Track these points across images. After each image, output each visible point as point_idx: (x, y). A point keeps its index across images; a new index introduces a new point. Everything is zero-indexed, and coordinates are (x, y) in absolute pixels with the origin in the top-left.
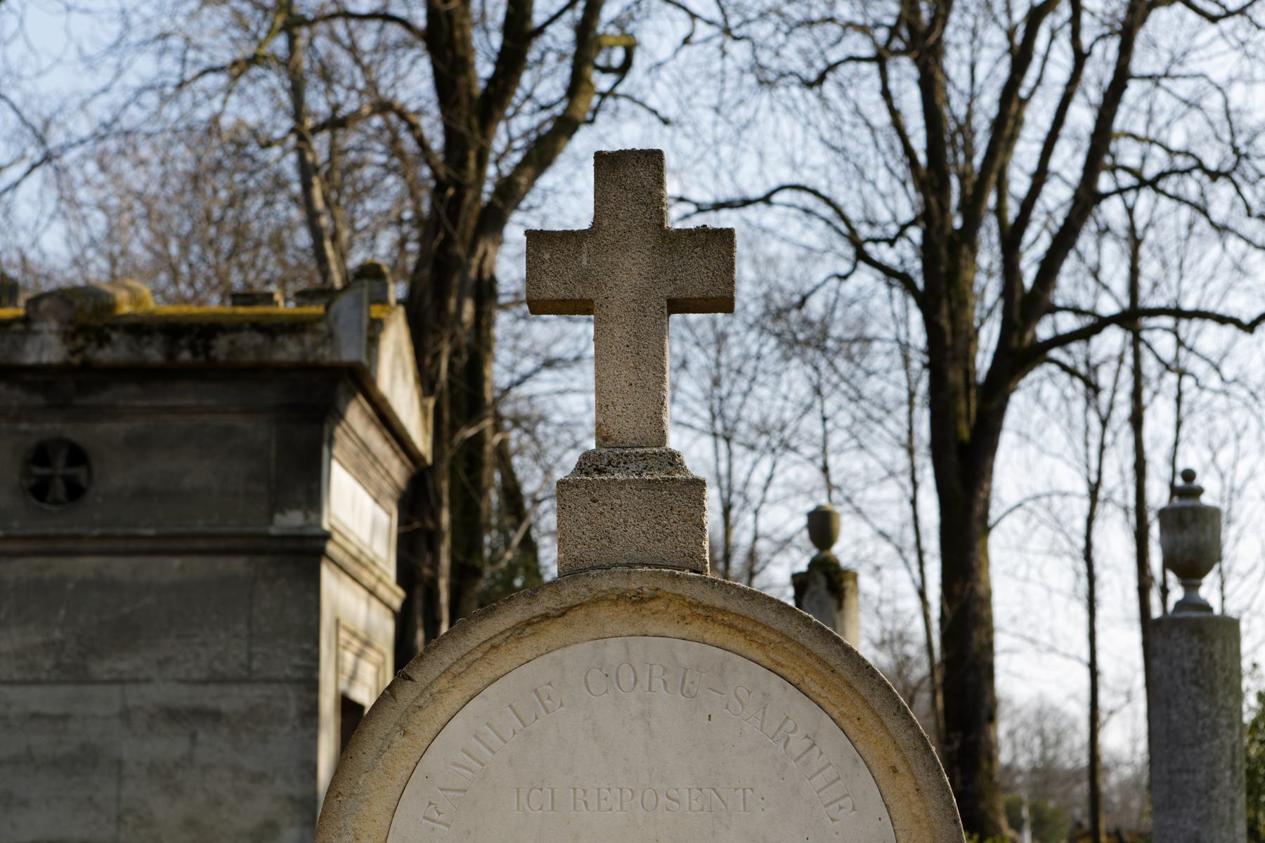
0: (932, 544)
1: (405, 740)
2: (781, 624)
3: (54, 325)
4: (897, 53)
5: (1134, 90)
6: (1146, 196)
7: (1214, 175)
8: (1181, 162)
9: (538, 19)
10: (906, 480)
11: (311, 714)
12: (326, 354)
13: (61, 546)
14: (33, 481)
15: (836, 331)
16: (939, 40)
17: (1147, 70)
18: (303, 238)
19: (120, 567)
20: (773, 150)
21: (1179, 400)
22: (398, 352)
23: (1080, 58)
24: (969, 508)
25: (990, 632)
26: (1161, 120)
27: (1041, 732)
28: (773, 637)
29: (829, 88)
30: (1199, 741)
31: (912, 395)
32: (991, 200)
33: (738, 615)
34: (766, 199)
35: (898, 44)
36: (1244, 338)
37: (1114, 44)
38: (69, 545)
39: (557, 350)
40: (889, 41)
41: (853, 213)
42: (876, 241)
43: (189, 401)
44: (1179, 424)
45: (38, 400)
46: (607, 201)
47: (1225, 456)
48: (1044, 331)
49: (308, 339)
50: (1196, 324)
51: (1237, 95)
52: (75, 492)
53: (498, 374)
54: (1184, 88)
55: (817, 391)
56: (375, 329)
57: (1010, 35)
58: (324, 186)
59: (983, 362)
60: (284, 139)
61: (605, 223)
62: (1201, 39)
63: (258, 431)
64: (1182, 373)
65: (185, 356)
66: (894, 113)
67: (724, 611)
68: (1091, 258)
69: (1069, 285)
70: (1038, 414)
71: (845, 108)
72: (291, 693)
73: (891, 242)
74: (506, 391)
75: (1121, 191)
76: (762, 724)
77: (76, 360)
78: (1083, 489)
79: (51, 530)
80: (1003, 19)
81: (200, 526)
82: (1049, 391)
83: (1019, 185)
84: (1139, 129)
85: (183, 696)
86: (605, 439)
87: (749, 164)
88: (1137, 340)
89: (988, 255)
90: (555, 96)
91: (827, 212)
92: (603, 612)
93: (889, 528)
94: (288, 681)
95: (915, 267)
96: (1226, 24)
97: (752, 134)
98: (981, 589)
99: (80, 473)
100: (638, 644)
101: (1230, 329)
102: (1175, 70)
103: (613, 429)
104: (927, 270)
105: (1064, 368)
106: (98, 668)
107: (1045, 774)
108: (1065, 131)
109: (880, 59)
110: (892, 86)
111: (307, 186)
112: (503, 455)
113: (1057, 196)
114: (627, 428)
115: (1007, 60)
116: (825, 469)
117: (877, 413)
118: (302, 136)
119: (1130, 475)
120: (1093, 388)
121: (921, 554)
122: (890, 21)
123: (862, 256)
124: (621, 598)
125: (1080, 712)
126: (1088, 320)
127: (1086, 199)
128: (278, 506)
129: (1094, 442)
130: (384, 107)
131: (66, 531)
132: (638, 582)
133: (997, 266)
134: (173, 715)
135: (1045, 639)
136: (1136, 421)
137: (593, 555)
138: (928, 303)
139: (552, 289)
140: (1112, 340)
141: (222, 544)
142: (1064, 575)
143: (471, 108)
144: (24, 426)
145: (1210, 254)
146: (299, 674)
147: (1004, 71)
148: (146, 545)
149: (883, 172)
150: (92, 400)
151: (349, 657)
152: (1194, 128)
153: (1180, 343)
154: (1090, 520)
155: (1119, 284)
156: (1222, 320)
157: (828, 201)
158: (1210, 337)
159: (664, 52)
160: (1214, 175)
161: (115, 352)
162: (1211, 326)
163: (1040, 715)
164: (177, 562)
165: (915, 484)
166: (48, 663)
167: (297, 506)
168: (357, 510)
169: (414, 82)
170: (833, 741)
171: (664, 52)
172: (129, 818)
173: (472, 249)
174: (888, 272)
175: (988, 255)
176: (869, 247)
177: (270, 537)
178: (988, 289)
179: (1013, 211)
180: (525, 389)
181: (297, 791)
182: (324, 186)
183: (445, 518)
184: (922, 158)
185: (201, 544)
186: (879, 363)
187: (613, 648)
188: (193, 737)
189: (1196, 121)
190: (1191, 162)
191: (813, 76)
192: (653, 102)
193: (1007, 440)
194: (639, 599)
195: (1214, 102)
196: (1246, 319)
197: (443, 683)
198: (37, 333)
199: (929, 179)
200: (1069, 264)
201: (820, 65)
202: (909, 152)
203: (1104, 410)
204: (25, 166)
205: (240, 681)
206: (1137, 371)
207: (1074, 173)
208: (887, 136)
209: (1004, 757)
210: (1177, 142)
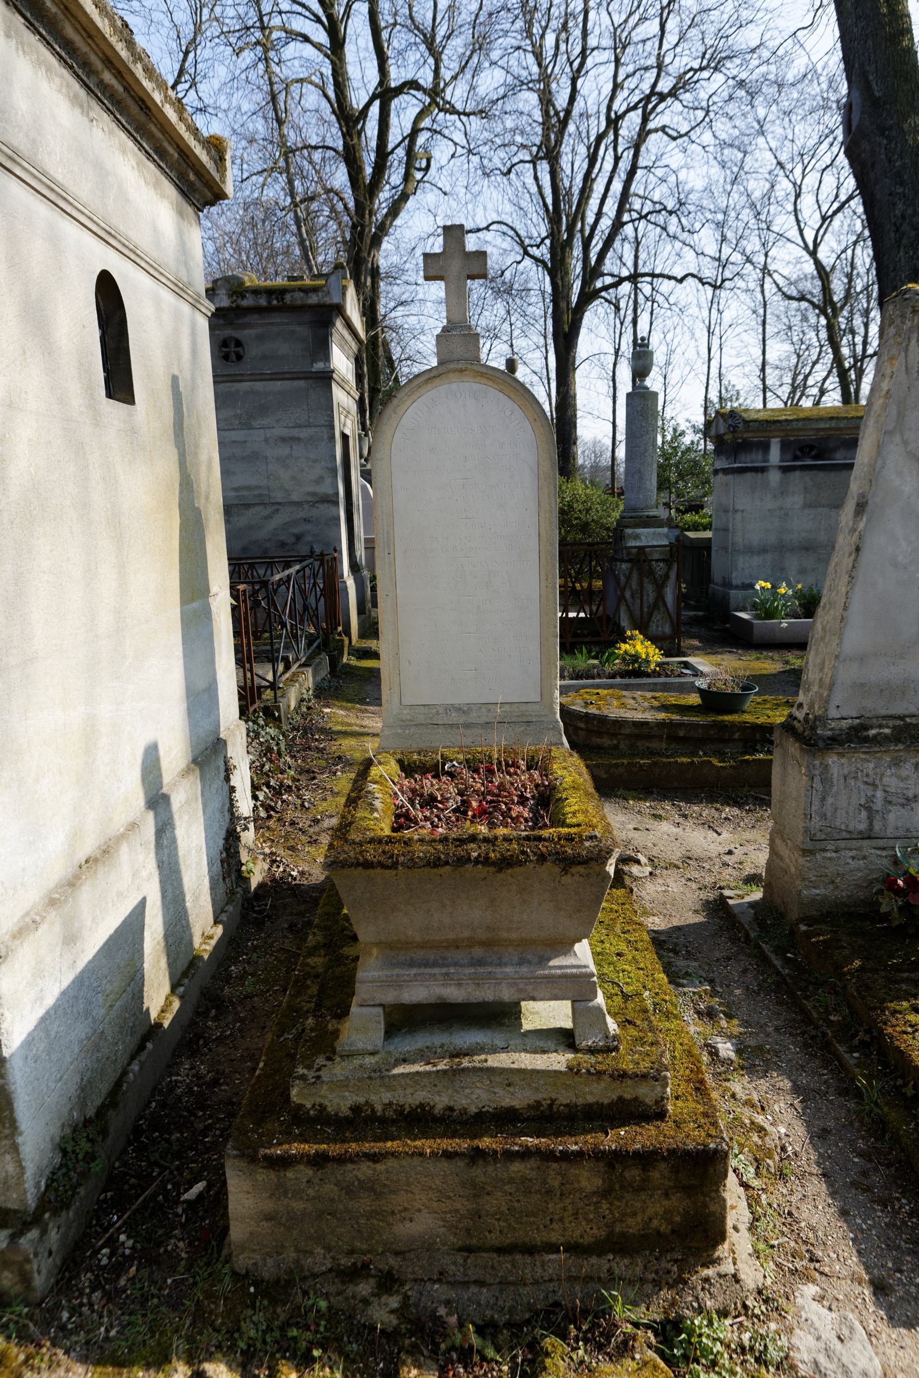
0: (553, 375)
2: (503, 377)
4: (541, 158)
5: (640, 173)
6: (643, 222)
7: (670, 213)
9: (390, 146)
10: (544, 350)
11: (333, 437)
12: (327, 300)
15: (516, 286)
16: (558, 152)
17: (644, 165)
18: (297, 251)
19: (259, 386)
20: (490, 206)
21: (652, 313)
23: (617, 159)
24: (567, 360)
25: (575, 410)
26: (650, 187)
27: (594, 452)
29: (512, 176)
30: (642, 436)
31: (546, 313)
32: (579, 225)
34: (487, 228)
36: (679, 286)
37: (632, 152)
39: (404, 298)
40: (538, 152)
41: (522, 233)
42: (532, 246)
44: (651, 324)
47: (669, 337)
48: (599, 284)
49: (320, 294)
50: (660, 279)
51: (682, 175)
52: (239, 357)
53: (381, 310)
55: (508, 312)
56: (344, 288)
57: (589, 148)
58: (305, 226)
59: (574, 299)
62: (669, 148)
63: (304, 331)
64: (653, 302)
65: (275, 302)
66: (540, 187)
69: (610, 265)
70: (596, 320)
71: (519, 184)
73: (538, 246)
74: (385, 316)
75: (633, 221)
76: (497, 402)
78: (612, 351)
80: (586, 140)
81: (286, 369)
82: (601, 310)
83: (590, 219)
84: (641, 193)
85: (286, 433)
87: (480, 212)
88: (636, 288)
89: (577, 251)
90: (398, 182)
91: (512, 233)
92: (451, 375)
93: (536, 370)
95: (547, 257)
96: (679, 141)
97: (481, 199)
98: (572, 393)
99: (239, 349)
101: (673, 282)
104: (552, 258)
105: (606, 300)
106: (255, 424)
107: (596, 468)
108: (610, 194)
109: (533, 162)
110: (539, 174)
111: (299, 228)
112: (386, 344)
113: (606, 223)
114: (456, 317)
116: (512, 346)
117: (532, 322)
120: (617, 308)
121: (549, 379)
122: (538, 143)
123: (526, 253)
124: (456, 370)
125: (609, 442)
127: (618, 225)
128: (314, 361)
129: (618, 332)
130: (328, 191)
132: (461, 365)
133: (581, 256)
134: (283, 440)
135: (595, 412)
136: (635, 322)
138: (552, 273)
139: (432, 273)
140: (626, 287)
142: (604, 387)
143: (365, 190)
145: (667, 248)
147: (585, 165)
149: (535, 214)
150: (241, 321)
151: (342, 417)
152: (664, 190)
153: (653, 289)
154: (615, 364)
155: (630, 264)
156: (670, 278)
157: (512, 228)
158: (666, 286)
159: (444, 162)
160: (670, 213)
162: (666, 281)
163: (595, 443)
164: (279, 383)
165: (547, 352)
168: (342, 362)
169: (340, 177)
170: (518, 412)
171: (444, 162)
173: (369, 254)
174: (536, 260)
175: (577, 251)
178: (576, 267)
179: (587, 233)
180: (393, 315)
181: (329, 465)
182: (305, 226)
183: (365, 369)
184: (551, 208)
185: (288, 376)
186: (533, 300)
187: (454, 386)
189: (664, 188)
192: (440, 185)
193: (583, 331)
194: (461, 371)
195: (672, 179)
199: (554, 218)
200: (610, 254)
201: (508, 165)
202: (545, 205)
205: (306, 426)
206: (636, 302)
207: (613, 214)
208: (537, 198)
209: (580, 461)
210: (656, 199)
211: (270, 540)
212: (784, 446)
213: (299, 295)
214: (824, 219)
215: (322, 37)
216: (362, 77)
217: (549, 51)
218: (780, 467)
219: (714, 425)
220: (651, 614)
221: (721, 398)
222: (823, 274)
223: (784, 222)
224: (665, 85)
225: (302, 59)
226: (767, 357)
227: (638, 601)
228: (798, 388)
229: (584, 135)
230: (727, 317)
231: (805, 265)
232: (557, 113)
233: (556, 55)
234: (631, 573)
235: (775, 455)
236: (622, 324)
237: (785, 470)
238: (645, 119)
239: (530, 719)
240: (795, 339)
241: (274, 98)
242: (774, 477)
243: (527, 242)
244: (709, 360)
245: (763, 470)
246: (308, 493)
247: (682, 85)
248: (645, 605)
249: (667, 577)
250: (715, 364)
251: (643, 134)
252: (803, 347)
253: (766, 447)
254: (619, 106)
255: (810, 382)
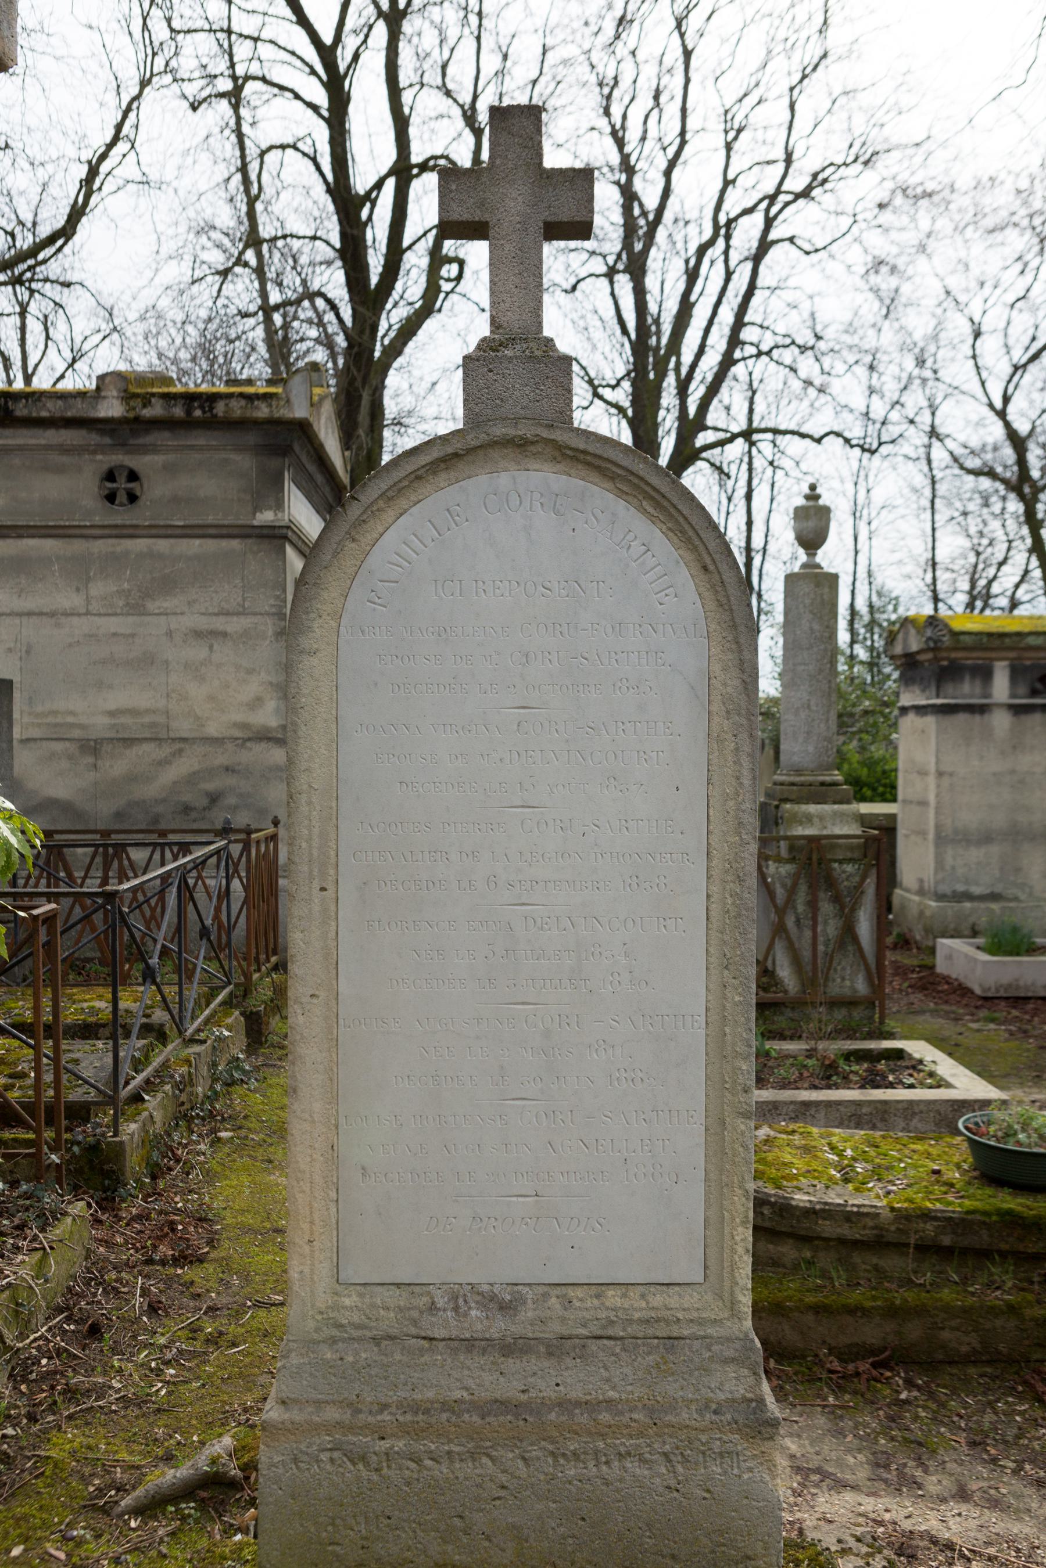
1: (353, 545)
3: (115, 393)
7: (803, 349)
8: (780, 340)
12: (284, 413)
13: (125, 532)
14: (107, 492)
19: (163, 545)
22: (329, 418)
23: (729, 275)
28: (619, 471)
33: (595, 456)
35: (620, 266)
37: (749, 265)
38: (131, 531)
43: (201, 442)
44: (772, 500)
45: (107, 440)
46: (499, 145)
52: (133, 498)
54: (788, 296)
57: (687, 261)
60: (256, 313)
61: (498, 162)
65: (198, 413)
67: (584, 452)
68: (726, 402)
69: (714, 416)
72: (269, 621)
73: (613, 387)
77: (131, 415)
79: (119, 522)
80: (683, 252)
81: (211, 519)
83: (687, 358)
85: (203, 623)
86: (498, 328)
89: (669, 398)
92: (495, 453)
94: (268, 614)
95: (626, 403)
100: (522, 476)
102: (782, 285)
103: (503, 320)
104: (633, 403)
106: (151, 606)
110: (616, 292)
113: (711, 361)
114: (513, 319)
115: (685, 277)
118: (267, 310)
119: (744, 528)
123: (596, 395)
126: (728, 435)
127: (727, 362)
128: (257, 509)
131: (128, 523)
134: (198, 634)
136: (749, 497)
137: (489, 412)
141: (224, 531)
144: (99, 457)
146: (274, 610)
147: (681, 286)
148: (178, 531)
150: (141, 441)
158: (793, 445)
161: (156, 410)
164: (197, 542)
166: (121, 603)
167: (270, 508)
169: (334, 281)
172: (173, 695)
176: (600, 390)
177: (254, 527)
178: (668, 421)
179: (684, 371)
187: (504, 480)
188: (211, 647)
190: (788, 341)
191: (569, 287)
196: (817, 436)
197: (381, 503)
198: (104, 398)
199: (640, 347)
200: (715, 401)
203: (730, 491)
204: (100, 336)
205: (238, 614)
211: (164, 800)
212: (1016, 673)
213: (236, 405)
214: (1016, 368)
215: (321, 97)
216: (371, 156)
217: (632, 136)
218: (1011, 707)
219: (900, 636)
220: (830, 957)
221: (871, 606)
222: (1018, 442)
223: (957, 370)
224: (796, 183)
225: (286, 120)
226: (937, 552)
227: (808, 933)
228: (979, 597)
229: (680, 245)
230: (878, 496)
231: (992, 428)
232: (644, 214)
233: (643, 139)
234: (795, 885)
235: (1001, 686)
236: (730, 499)
237: (1018, 710)
238: (769, 223)
239: (675, 1331)
240: (973, 530)
241: (243, 169)
242: (1001, 721)
243: (596, 382)
244: (857, 552)
245: (982, 709)
246: (236, 725)
247: (818, 181)
248: (821, 939)
249: (858, 891)
250: (862, 559)
251: (764, 246)
252: (985, 542)
253: (985, 674)
254: (733, 205)
255: (995, 589)
